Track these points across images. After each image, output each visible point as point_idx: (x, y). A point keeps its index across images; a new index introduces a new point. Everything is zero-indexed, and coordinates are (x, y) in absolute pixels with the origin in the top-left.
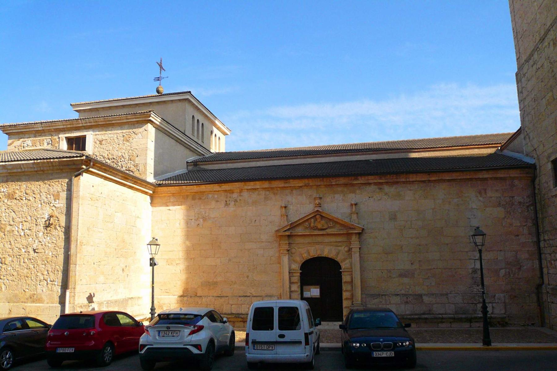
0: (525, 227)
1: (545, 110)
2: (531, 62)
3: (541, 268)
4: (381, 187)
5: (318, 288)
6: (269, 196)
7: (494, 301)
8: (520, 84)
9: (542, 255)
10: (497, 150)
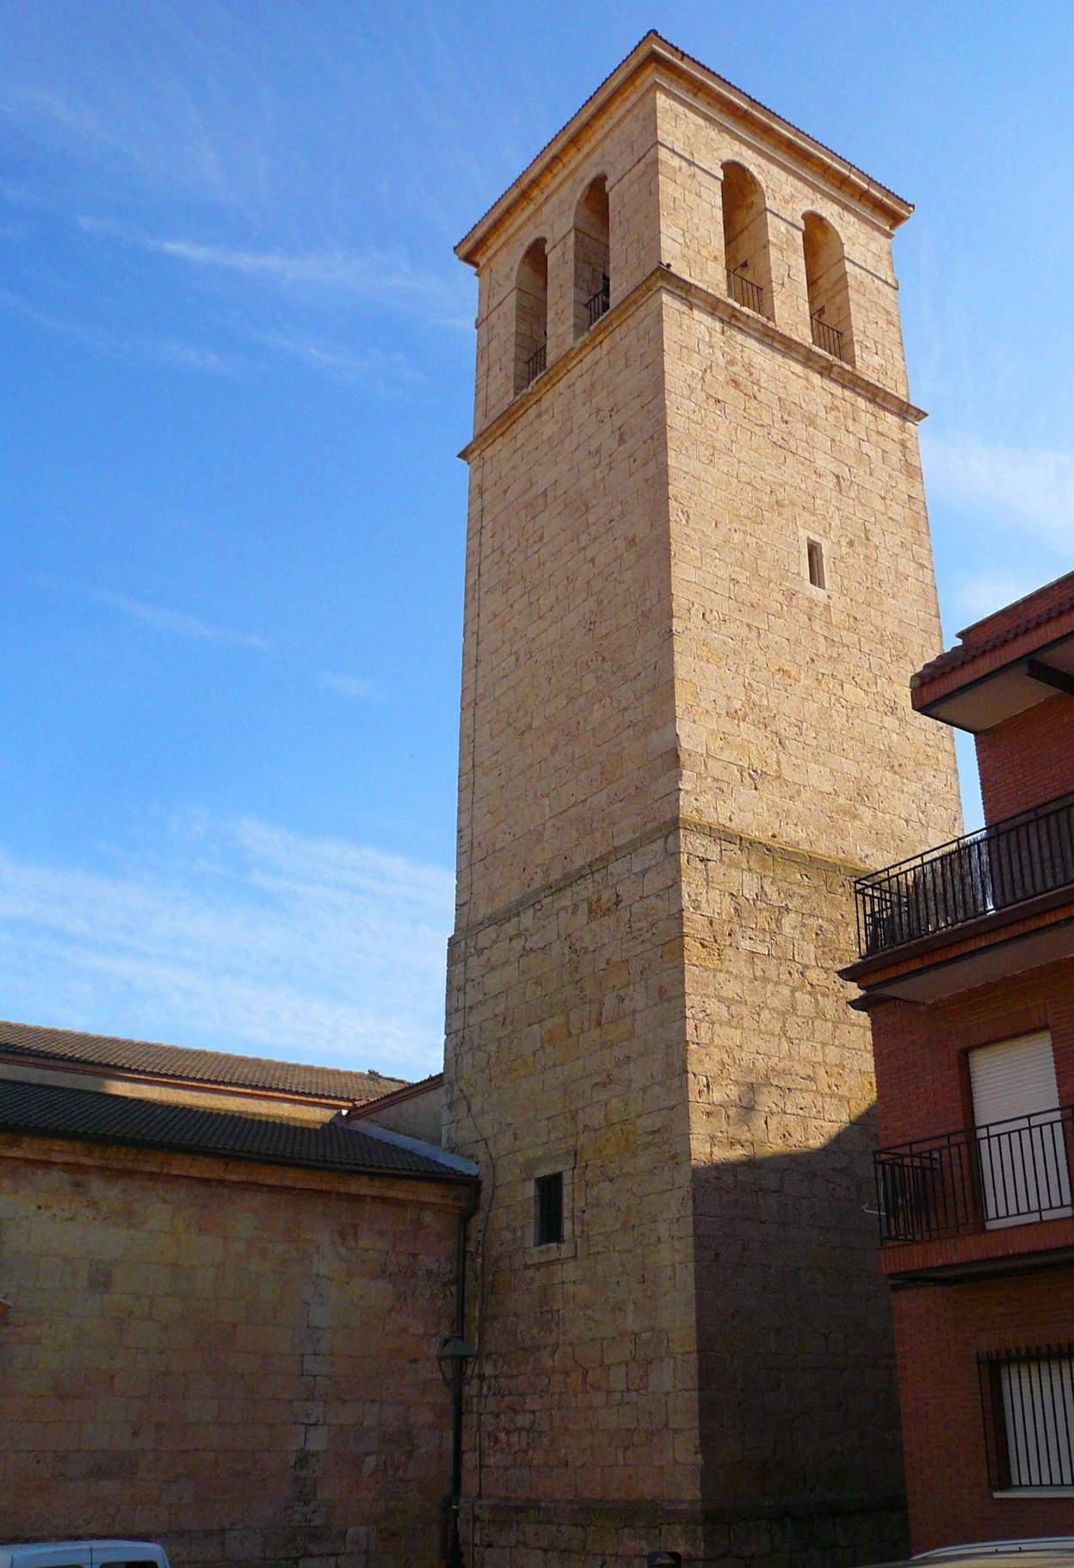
0: (434, 1340)
1: (534, 1053)
2: (510, 928)
3: (458, 1454)
4: (79, 1177)
7: (342, 1550)
8: (460, 967)
9: (464, 1417)
10: (337, 1115)
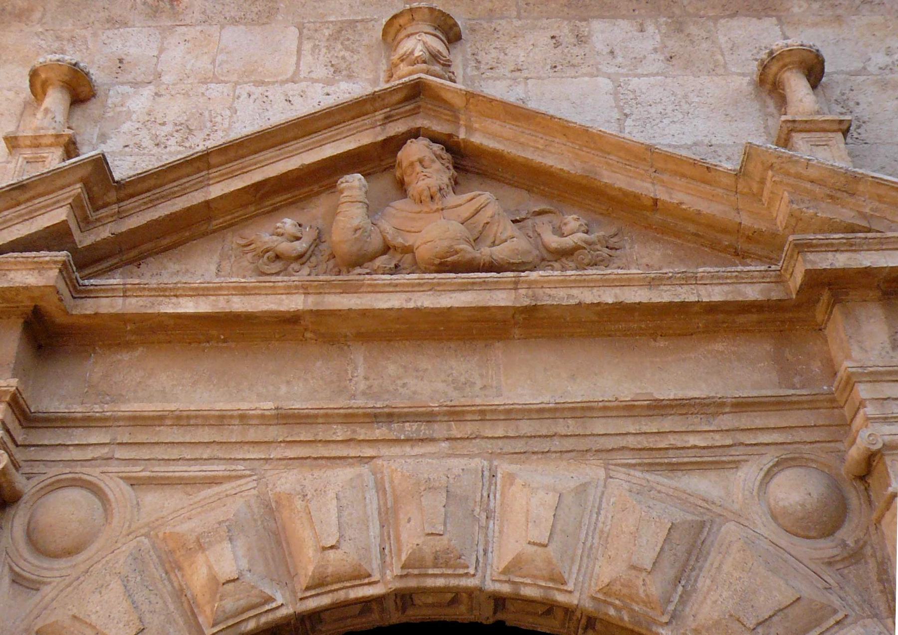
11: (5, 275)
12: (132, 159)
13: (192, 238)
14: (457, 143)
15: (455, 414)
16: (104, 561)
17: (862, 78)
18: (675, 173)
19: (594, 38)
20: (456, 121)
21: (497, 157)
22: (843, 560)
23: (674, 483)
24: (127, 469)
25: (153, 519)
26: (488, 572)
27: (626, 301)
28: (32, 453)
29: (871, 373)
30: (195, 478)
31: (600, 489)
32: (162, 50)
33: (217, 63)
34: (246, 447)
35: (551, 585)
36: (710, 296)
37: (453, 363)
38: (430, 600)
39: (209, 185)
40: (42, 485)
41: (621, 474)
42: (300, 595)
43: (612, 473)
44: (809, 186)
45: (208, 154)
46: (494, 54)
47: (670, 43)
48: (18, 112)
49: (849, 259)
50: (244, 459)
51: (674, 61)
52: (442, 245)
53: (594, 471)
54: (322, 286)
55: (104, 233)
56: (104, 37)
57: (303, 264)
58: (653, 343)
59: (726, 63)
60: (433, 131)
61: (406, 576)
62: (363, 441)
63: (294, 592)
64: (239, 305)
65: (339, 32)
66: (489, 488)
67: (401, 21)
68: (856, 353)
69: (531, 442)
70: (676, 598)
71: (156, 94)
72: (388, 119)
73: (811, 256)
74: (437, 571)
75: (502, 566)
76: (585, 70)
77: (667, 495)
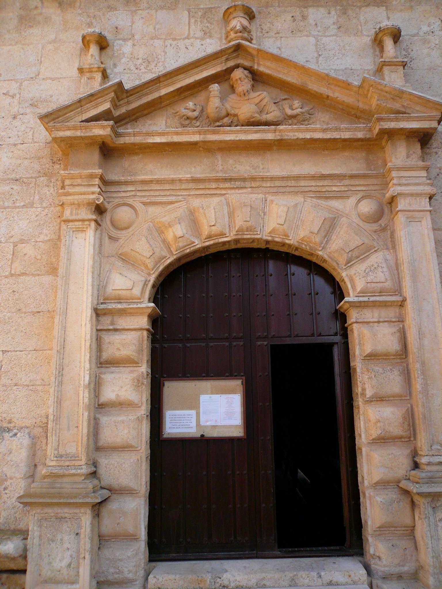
5: (232, 391)
6: (39, 11)
11: (91, 130)
12: (128, 75)
13: (155, 110)
14: (254, 70)
15: (253, 179)
16: (138, 231)
17: (416, 38)
18: (336, 85)
19: (309, 17)
20: (253, 61)
21: (269, 76)
22: (380, 230)
23: (327, 203)
24: (142, 199)
25: (152, 216)
26: (264, 233)
27: (315, 138)
28: (109, 195)
29: (397, 168)
30: (165, 202)
31: (302, 205)
32: (133, 23)
33: (156, 29)
34: (182, 191)
35: (284, 237)
36: (344, 136)
37: (252, 159)
38: (245, 242)
39: (160, 89)
40: (113, 206)
41: (309, 200)
42: (203, 241)
43: (306, 200)
44: (385, 94)
45: (159, 77)
46: (268, 25)
47: (340, 20)
48: (79, 53)
49: (396, 124)
50: (181, 195)
51: (341, 29)
52: (248, 115)
53: (300, 199)
54: (205, 132)
55: (123, 110)
56: (108, 16)
57: (198, 120)
58: (323, 152)
59: (362, 30)
60: (245, 65)
61: (238, 234)
62: (222, 188)
63: (201, 240)
64: (176, 139)
65: (205, 14)
66: (265, 205)
67: (231, 10)
68: (393, 160)
69: (279, 188)
70: (324, 242)
71: (133, 45)
72: (227, 60)
73: (382, 123)
74: (247, 233)
75: (269, 231)
76: (305, 33)
77: (324, 207)
